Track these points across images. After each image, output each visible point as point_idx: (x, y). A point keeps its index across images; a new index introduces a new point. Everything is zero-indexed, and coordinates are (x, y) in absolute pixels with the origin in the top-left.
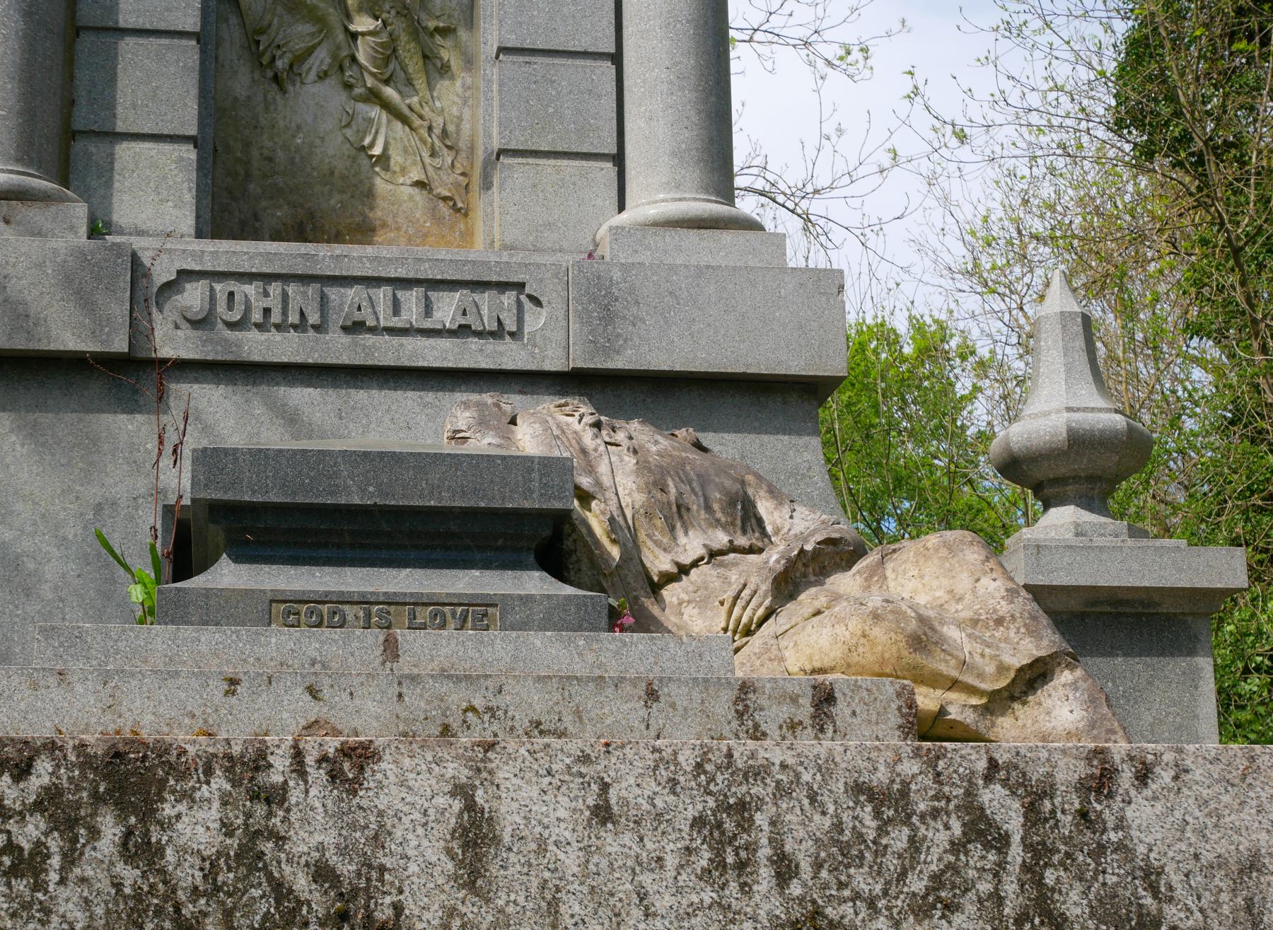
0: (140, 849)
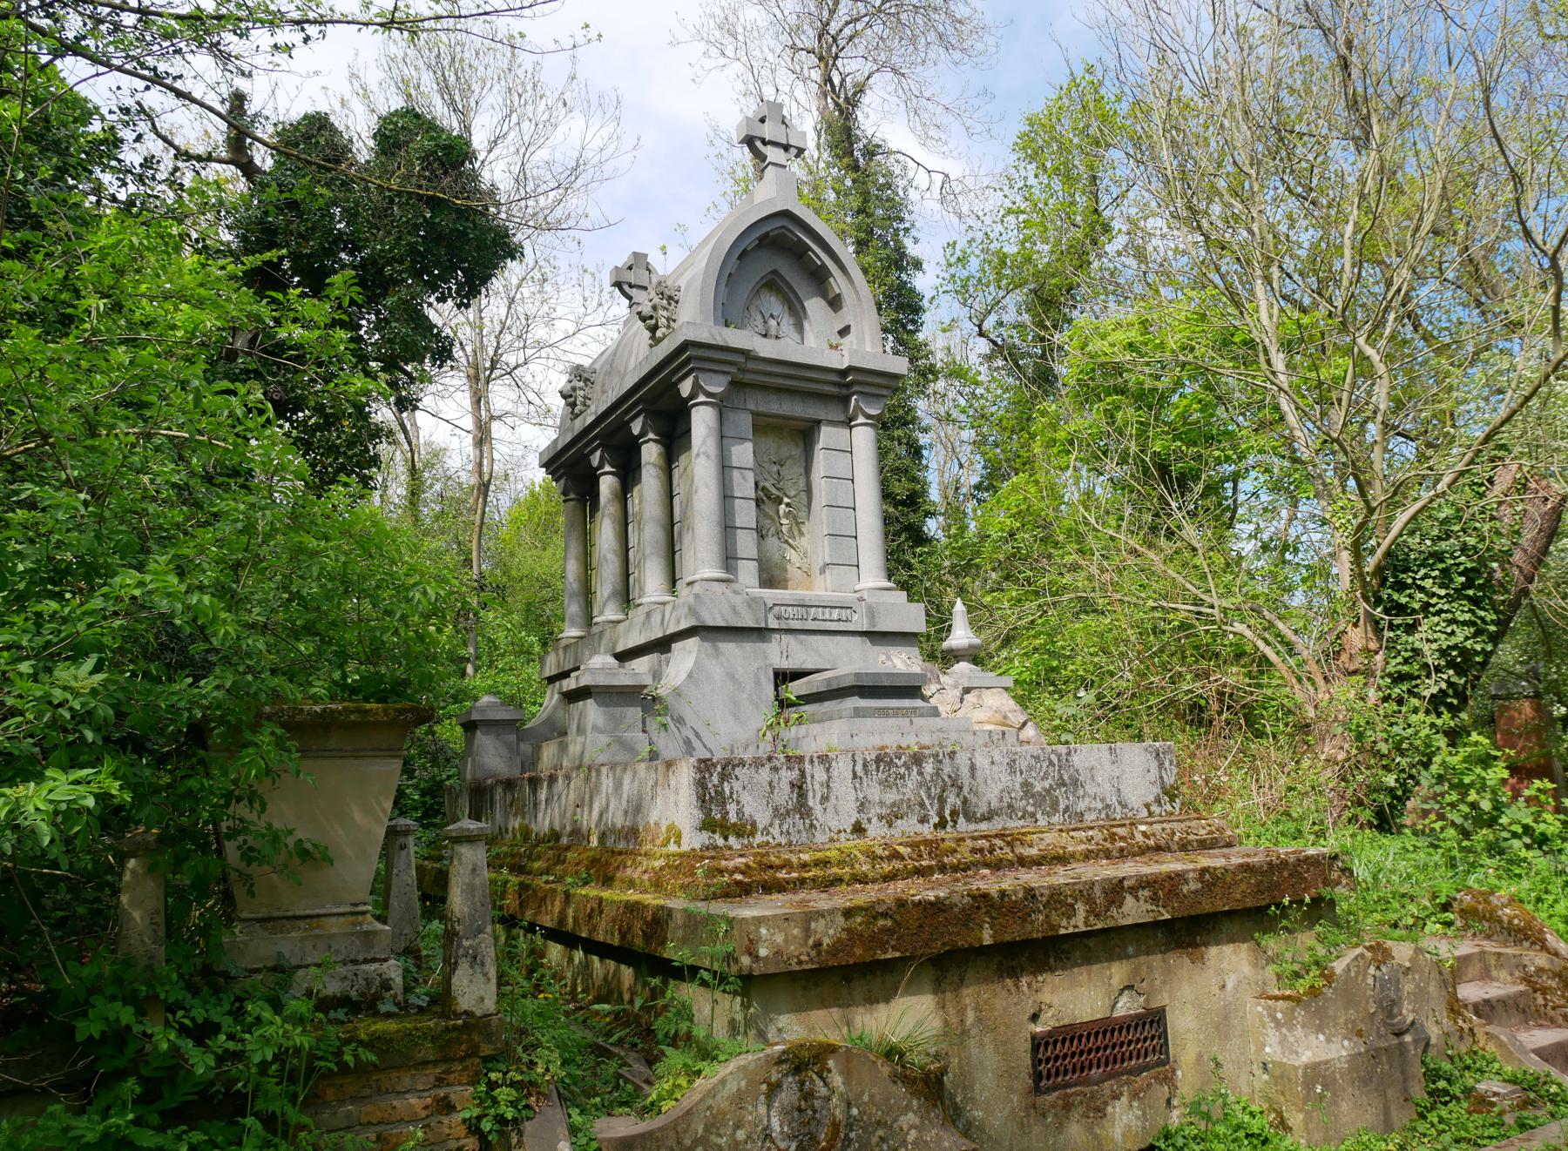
0: (920, 773)
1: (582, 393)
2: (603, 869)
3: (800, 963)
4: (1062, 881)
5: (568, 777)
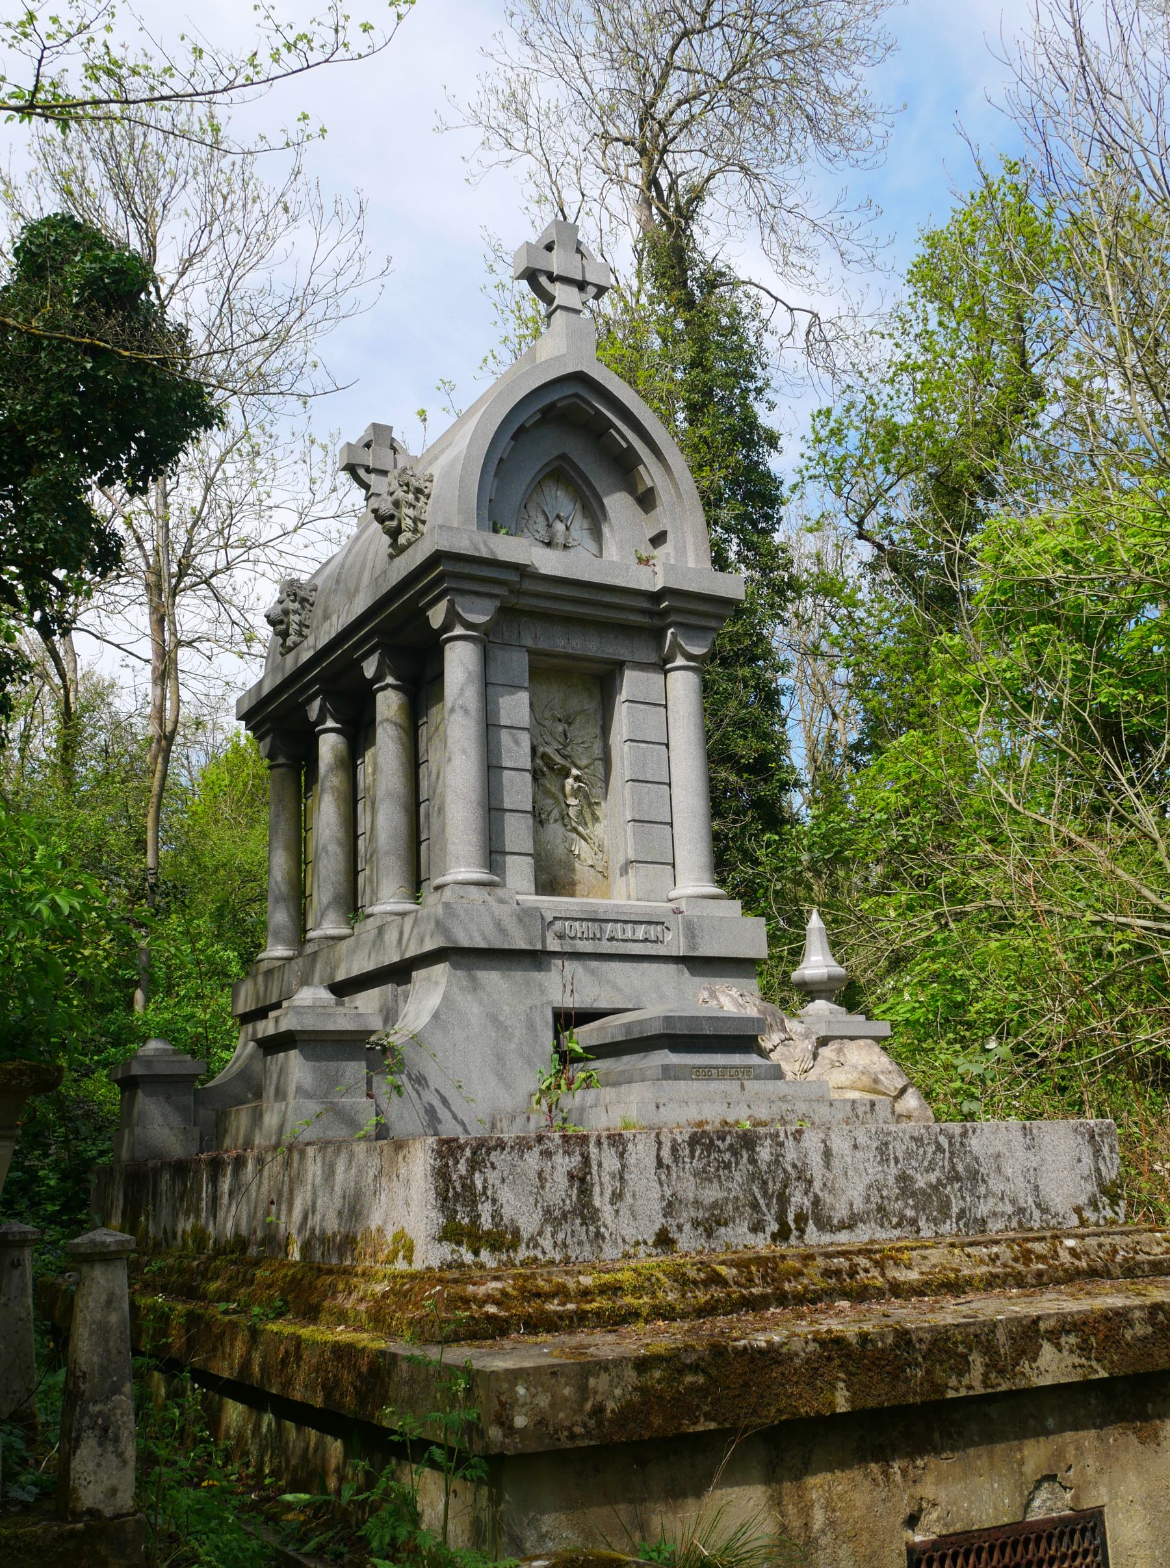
0: (753, 1161)
1: (296, 618)
2: (306, 1294)
3: (572, 1437)
4: (950, 1320)
5: (260, 1161)
